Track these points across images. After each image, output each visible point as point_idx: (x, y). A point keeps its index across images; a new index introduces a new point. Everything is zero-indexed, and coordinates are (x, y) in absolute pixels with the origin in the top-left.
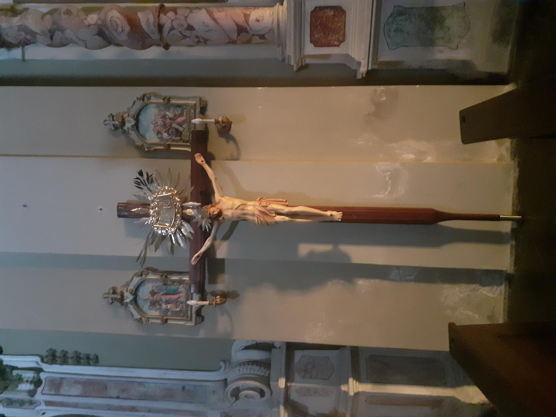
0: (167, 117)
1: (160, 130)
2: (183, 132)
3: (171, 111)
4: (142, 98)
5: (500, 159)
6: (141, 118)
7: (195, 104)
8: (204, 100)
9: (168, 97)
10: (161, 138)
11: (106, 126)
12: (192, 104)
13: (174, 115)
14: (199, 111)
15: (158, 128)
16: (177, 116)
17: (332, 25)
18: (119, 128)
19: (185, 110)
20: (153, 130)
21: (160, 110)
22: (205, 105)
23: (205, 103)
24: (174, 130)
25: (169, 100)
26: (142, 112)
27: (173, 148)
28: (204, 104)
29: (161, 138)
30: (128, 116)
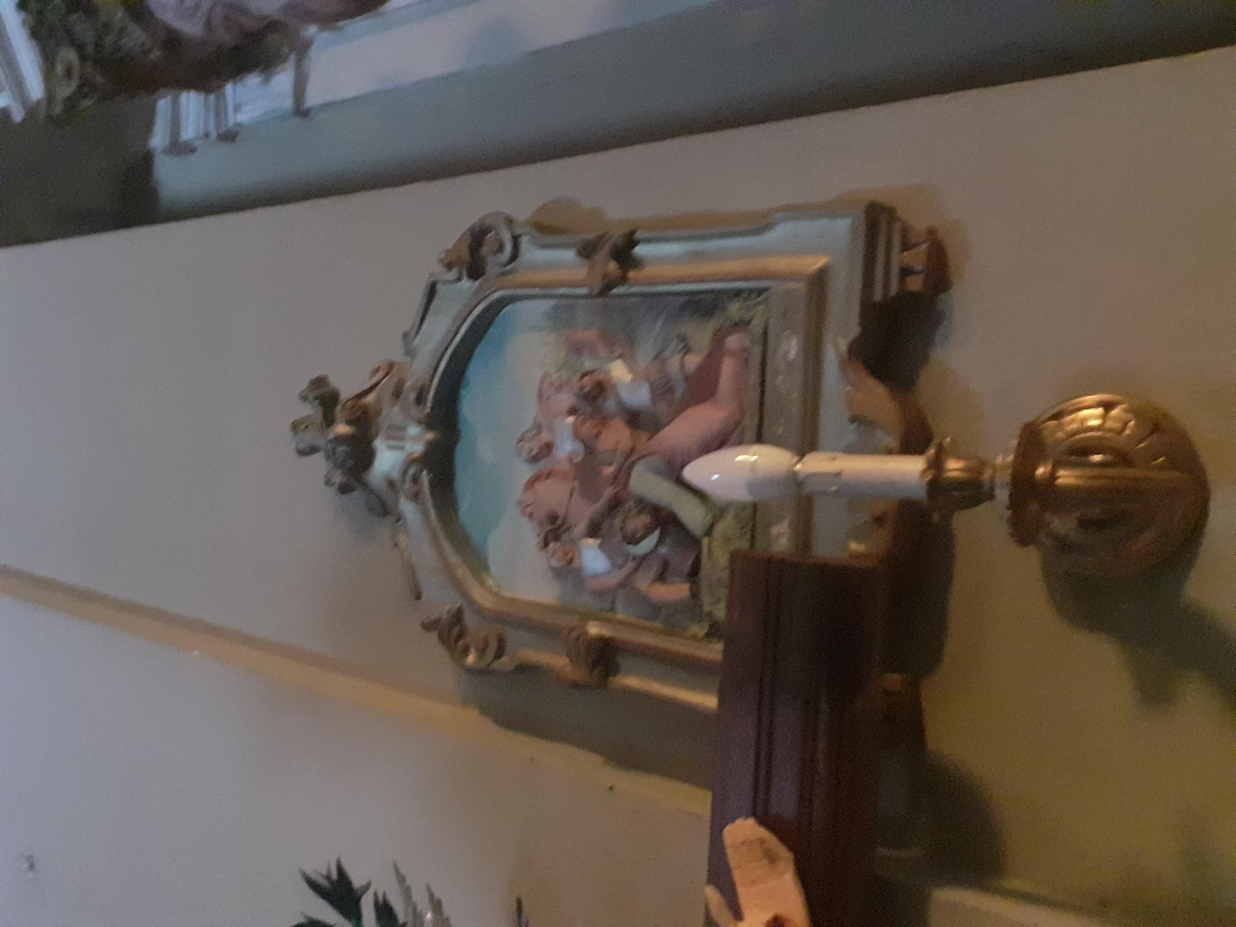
0: (610, 404)
1: (561, 512)
2: (705, 542)
3: (645, 352)
4: (466, 255)
5: (96, 81)
6: (471, 406)
7: (819, 282)
8: (920, 223)
9: (617, 235)
10: (568, 571)
11: (308, 459)
12: (791, 276)
13: (653, 388)
14: (843, 345)
15: (555, 494)
16: (679, 393)
17: (1133, 559)
18: (613, 417)
19: (733, 341)
20: (524, 507)
21: (577, 349)
22: (915, 284)
23: (917, 258)
24: (639, 522)
25: (624, 254)
26: (475, 370)
27: (632, 681)
28: (906, 272)
29: (568, 571)
30: (397, 393)
